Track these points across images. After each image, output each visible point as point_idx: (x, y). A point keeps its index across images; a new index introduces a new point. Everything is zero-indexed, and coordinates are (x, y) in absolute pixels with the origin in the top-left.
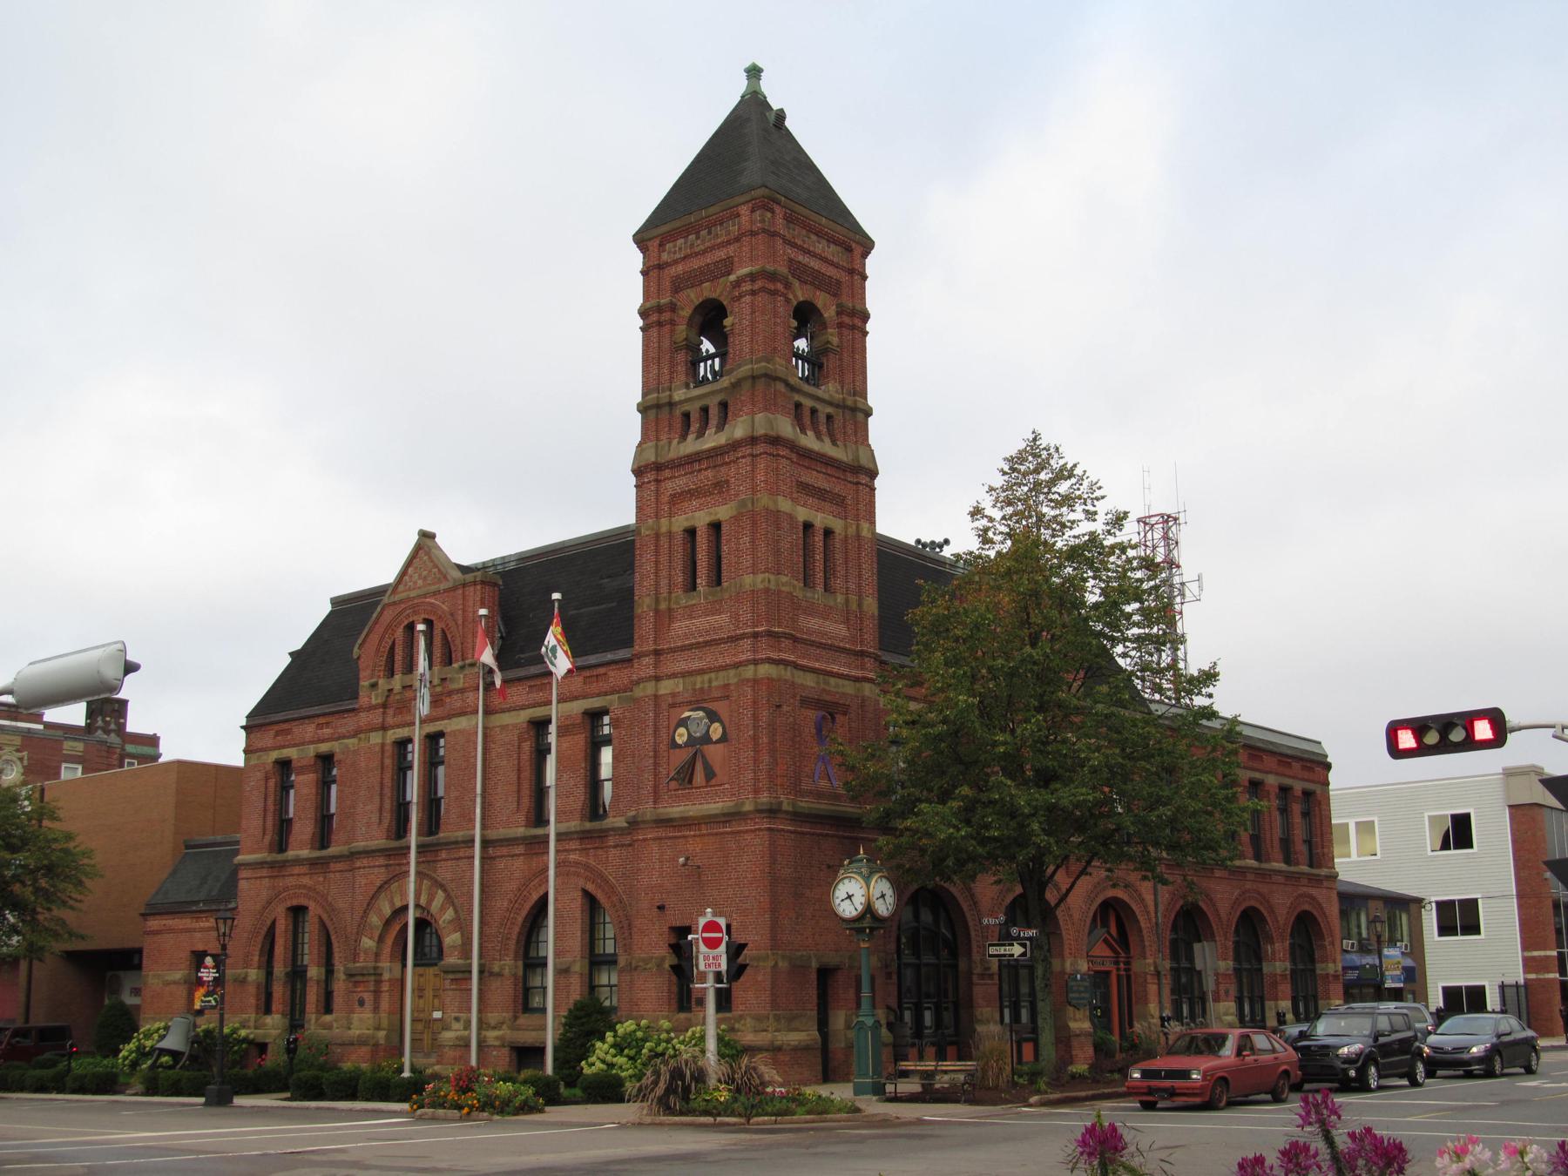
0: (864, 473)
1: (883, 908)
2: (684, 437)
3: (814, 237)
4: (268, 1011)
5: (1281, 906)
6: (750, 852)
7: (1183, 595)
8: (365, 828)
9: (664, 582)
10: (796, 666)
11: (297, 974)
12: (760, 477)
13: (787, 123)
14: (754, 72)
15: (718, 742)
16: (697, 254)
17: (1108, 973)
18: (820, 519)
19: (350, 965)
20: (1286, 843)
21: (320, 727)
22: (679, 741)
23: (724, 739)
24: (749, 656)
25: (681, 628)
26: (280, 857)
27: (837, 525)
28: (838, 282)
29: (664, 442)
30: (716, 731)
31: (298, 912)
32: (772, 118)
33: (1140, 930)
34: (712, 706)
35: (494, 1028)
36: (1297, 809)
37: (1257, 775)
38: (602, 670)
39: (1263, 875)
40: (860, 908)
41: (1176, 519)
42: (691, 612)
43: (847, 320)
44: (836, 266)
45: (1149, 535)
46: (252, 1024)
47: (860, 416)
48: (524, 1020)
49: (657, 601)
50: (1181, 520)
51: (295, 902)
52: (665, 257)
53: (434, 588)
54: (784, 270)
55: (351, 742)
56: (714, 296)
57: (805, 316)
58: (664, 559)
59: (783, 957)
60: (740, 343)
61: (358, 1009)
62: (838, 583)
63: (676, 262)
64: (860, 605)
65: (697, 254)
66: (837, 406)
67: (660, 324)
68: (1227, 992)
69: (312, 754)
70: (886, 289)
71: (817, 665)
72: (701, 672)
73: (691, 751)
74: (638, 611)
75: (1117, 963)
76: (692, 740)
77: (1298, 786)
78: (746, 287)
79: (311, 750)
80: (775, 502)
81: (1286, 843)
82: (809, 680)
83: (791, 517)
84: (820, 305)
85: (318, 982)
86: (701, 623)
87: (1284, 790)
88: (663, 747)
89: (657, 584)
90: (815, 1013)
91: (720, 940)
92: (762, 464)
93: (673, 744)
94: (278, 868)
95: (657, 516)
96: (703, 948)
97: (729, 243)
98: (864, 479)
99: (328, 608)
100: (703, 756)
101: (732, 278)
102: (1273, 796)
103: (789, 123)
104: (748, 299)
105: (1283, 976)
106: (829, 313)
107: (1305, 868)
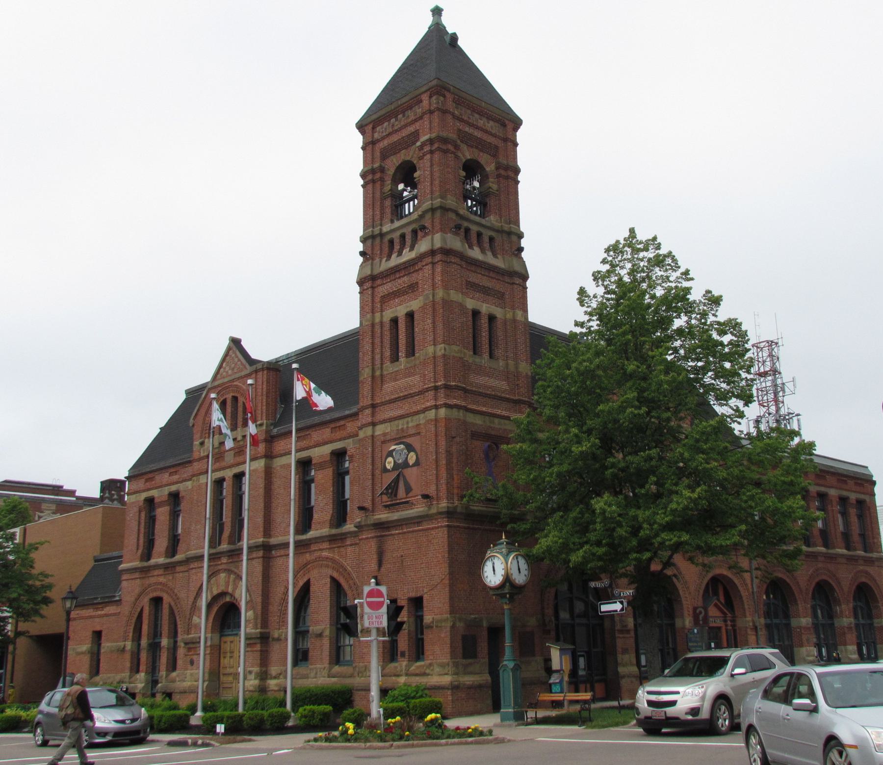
0: (518, 277)
1: (520, 578)
2: (389, 257)
3: (477, 116)
4: (138, 671)
5: (845, 579)
6: (437, 541)
7: (783, 390)
8: (199, 540)
9: (378, 357)
10: (467, 409)
11: (154, 647)
12: (438, 278)
13: (460, 43)
14: (437, 12)
15: (414, 465)
16: (396, 131)
17: (719, 628)
18: (485, 308)
19: (186, 636)
20: (846, 536)
21: (171, 474)
22: (389, 466)
23: (417, 463)
24: (432, 403)
25: (389, 389)
26: (145, 564)
27: (498, 312)
28: (496, 147)
29: (377, 260)
30: (412, 458)
31: (157, 601)
32: (448, 39)
33: (741, 597)
34: (408, 440)
35: (275, 678)
36: (853, 512)
37: (822, 489)
38: (342, 423)
39: (831, 558)
40: (501, 578)
41: (777, 344)
42: (395, 377)
43: (502, 172)
44: (495, 136)
45: (760, 354)
46: (127, 680)
47: (514, 238)
48: (337, 669)
49: (373, 370)
50: (780, 344)
51: (155, 594)
52: (376, 136)
53: (237, 375)
54: (453, 136)
55: (189, 484)
56: (408, 159)
57: (472, 169)
58: (377, 341)
59: (460, 620)
60: (425, 186)
61: (189, 666)
62: (499, 352)
63: (383, 138)
64: (517, 368)
65: (396, 131)
66: (497, 231)
67: (373, 181)
68: (808, 640)
69: (166, 493)
70: (530, 150)
71: (484, 409)
72: (401, 417)
73: (396, 473)
74: (361, 378)
75: (725, 621)
76: (396, 466)
77: (853, 497)
78: (427, 148)
79: (166, 491)
80: (449, 294)
81: (846, 536)
82: (478, 420)
83: (462, 306)
84: (483, 162)
85: (168, 649)
86: (402, 383)
87: (843, 500)
88: (378, 472)
89: (373, 358)
90: (487, 660)
91: (383, 603)
92: (439, 268)
93: (385, 470)
94: (145, 571)
95: (373, 312)
96: (367, 609)
97: (416, 121)
98: (518, 281)
99: (184, 397)
100: (404, 477)
101: (418, 144)
102: (834, 503)
103: (460, 43)
104: (428, 156)
105: (850, 628)
106: (490, 168)
107: (861, 553)
